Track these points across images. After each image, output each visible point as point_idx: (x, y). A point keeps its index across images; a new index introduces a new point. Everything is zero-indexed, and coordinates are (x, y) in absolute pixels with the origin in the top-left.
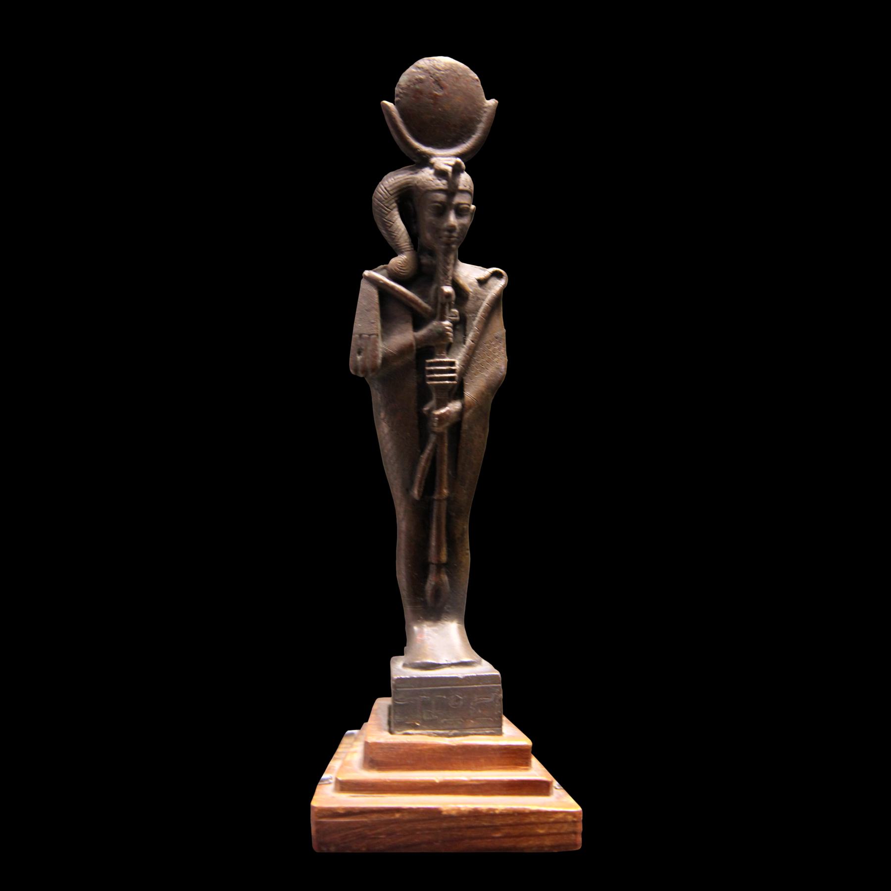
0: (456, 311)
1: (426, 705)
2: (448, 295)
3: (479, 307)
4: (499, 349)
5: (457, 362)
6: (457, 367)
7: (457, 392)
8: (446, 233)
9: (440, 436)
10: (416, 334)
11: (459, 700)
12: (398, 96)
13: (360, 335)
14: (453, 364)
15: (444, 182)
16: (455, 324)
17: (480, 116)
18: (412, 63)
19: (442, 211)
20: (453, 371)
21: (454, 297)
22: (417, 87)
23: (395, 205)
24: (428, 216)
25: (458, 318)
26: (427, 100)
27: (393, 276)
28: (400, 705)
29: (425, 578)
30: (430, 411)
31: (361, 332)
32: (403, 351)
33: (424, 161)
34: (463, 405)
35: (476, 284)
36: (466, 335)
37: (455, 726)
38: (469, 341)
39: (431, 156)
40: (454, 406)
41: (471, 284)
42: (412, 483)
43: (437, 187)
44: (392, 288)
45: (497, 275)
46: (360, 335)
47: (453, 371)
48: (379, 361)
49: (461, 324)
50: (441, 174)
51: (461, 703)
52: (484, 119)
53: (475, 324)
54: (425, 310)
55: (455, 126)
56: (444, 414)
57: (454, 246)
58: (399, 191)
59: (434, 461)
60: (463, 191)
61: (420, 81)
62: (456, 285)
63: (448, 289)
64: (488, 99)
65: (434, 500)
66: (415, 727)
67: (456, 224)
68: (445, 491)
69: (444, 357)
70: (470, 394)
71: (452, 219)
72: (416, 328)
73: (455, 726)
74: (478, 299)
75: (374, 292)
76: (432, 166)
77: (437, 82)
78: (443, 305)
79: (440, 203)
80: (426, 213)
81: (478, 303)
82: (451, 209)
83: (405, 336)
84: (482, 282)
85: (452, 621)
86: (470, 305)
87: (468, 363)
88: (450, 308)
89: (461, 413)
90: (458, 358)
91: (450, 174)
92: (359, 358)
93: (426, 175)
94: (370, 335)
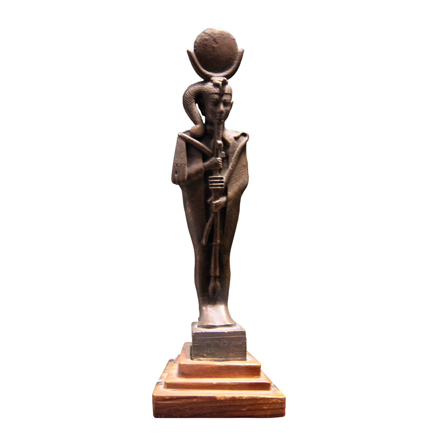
0: (224, 152)
1: (209, 346)
2: (220, 145)
3: (235, 151)
5: (224, 178)
6: (224, 180)
7: (224, 192)
8: (219, 114)
9: (216, 214)
10: (204, 164)
11: (225, 343)
14: (222, 178)
15: (218, 89)
16: (223, 159)
17: (235, 57)
19: (217, 103)
20: (222, 182)
21: (223, 146)
22: (205, 43)
23: (194, 100)
25: (225, 156)
26: (210, 49)
28: (196, 346)
29: (208, 283)
30: (211, 202)
31: (177, 163)
32: (198, 172)
33: (207, 79)
34: (227, 199)
35: (234, 139)
36: (228, 164)
37: (223, 356)
38: (230, 167)
39: (211, 76)
40: (223, 199)
41: (231, 139)
42: (202, 237)
43: (215, 92)
44: (192, 141)
47: (222, 182)
48: (186, 177)
49: (226, 159)
51: (226, 345)
53: (233, 159)
54: (209, 152)
55: (223, 62)
56: (218, 203)
58: (196, 94)
59: (213, 226)
60: (227, 94)
61: (206, 40)
62: (224, 140)
63: (220, 142)
65: (213, 245)
66: (204, 357)
67: (224, 110)
68: (218, 241)
69: (218, 175)
70: (230, 193)
72: (204, 161)
73: (223, 356)
74: (235, 147)
77: (215, 40)
78: (217, 150)
79: (216, 99)
80: (209, 105)
81: (235, 149)
82: (221, 103)
83: (198, 165)
85: (222, 304)
86: (230, 150)
87: (229, 178)
88: (221, 151)
89: (226, 203)
90: (224, 176)
91: (221, 85)
93: (209, 86)
94: (181, 164)
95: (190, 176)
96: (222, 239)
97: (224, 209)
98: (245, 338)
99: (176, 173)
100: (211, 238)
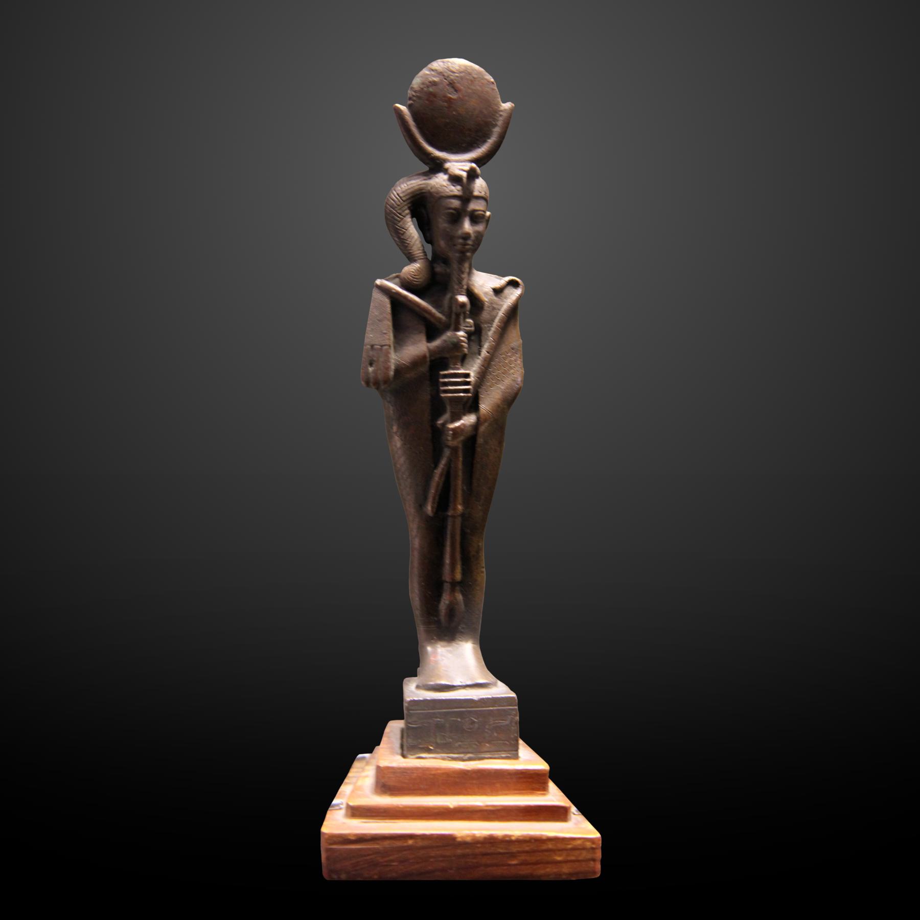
0: (471, 321)
1: (440, 727)
2: (463, 305)
3: (495, 317)
4: (516, 360)
5: (472, 374)
6: (471, 379)
7: (472, 405)
8: (461, 241)
9: (454, 450)
10: (429, 345)
11: (473, 722)
13: (372, 346)
14: (467, 376)
15: (459, 187)
16: (470, 335)
17: (495, 120)
19: (456, 217)
20: (468, 383)
21: (469, 307)
22: (431, 89)
23: (407, 211)
24: (442, 224)
25: (473, 329)
26: (441, 103)
27: (406, 285)
28: (413, 728)
29: (438, 596)
30: (444, 425)
31: (373, 343)
32: (417, 363)
33: (437, 166)
34: (478, 419)
35: (492, 293)
36: (481, 346)
37: (470, 750)
38: (484, 352)
39: (445, 161)
40: (469, 420)
41: (486, 293)
42: (425, 498)
43: (452, 193)
44: (405, 297)
46: (372, 346)
47: (468, 383)
48: (392, 373)
49: (476, 335)
51: (476, 726)
53: (490, 334)
54: (439, 320)
55: (470, 130)
56: (459, 427)
58: (412, 197)
59: (448, 476)
60: (478, 198)
61: (434, 84)
62: (471, 294)
63: (463, 299)
65: (448, 516)
66: (429, 751)
67: (471, 232)
68: (460, 507)
69: (458, 369)
70: (485, 407)
71: (467, 226)
72: (430, 338)
73: (470, 750)
74: (494, 309)
75: (387, 302)
76: (446, 171)
77: (452, 84)
78: (458, 315)
79: (455, 209)
80: (440, 220)
81: (494, 313)
82: (465, 216)
83: (418, 347)
84: (498, 291)
85: (467, 641)
86: (485, 315)
87: (483, 375)
88: (465, 318)
89: (476, 427)
90: (472, 370)
91: (465, 180)
92: (371, 369)
93: (440, 180)
94: (382, 346)
96: (466, 503)
97: (471, 439)
99: (371, 364)
100: (444, 502)
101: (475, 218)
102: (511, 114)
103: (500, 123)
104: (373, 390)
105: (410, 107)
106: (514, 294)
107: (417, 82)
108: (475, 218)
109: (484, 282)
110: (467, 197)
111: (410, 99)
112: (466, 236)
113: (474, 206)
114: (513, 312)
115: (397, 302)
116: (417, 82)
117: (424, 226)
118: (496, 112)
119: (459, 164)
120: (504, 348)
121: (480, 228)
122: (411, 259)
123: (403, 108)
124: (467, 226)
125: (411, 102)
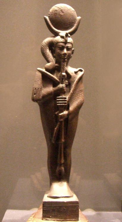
0: (67, 81)
1: (53, 210)
2: (64, 76)
3: (75, 80)
4: (82, 94)
5: (67, 98)
6: (67, 99)
7: (67, 108)
8: (63, 56)
9: (61, 122)
10: (53, 88)
11: (64, 209)
12: (47, 48)
13: (35, 88)
14: (65, 98)
15: (63, 39)
16: (67, 86)
17: (75, 21)
18: (54, 6)
19: (62, 48)
20: (66, 101)
21: (66, 76)
22: (55, 12)
23: (48, 47)
24: (58, 51)
25: (68, 84)
26: (58, 16)
27: (47, 70)
28: (45, 210)
29: (56, 168)
30: (58, 114)
31: (36, 87)
32: (50, 94)
33: (56, 34)
34: (69, 112)
35: (74, 73)
36: (70, 89)
37: (63, 218)
38: (71, 91)
39: (59, 33)
40: (65, 112)
41: (72, 73)
42: (52, 136)
43: (61, 41)
44: (46, 73)
45: (81, 71)
46: (35, 88)
47: (66, 101)
48: (41, 97)
49: (69, 85)
50: (62, 37)
51: (65, 210)
52: (76, 22)
53: (73, 86)
54: (57, 81)
55: (67, 24)
56: (62, 115)
57: (66, 60)
58: (49, 43)
59: (59, 130)
60: (69, 43)
61: (56, 10)
62: (67, 72)
63: (64, 74)
64: (78, 17)
65: (59, 143)
66: (49, 218)
67: (67, 53)
68: (63, 140)
69: (63, 96)
70: (71, 108)
71: (65, 51)
72: (54, 86)
73: (63, 218)
74: (75, 78)
75: (40, 74)
76: (60, 35)
77: (62, 11)
78: (63, 79)
79: (62, 46)
80: (57, 49)
81: (75, 79)
82: (65, 48)
83: (50, 89)
84: (76, 73)
85: (65, 182)
86: (71, 80)
87: (71, 98)
88: (65, 80)
89: (68, 115)
90: (67, 97)
91: (65, 37)
92: (35, 96)
93: (58, 39)
94: (38, 88)
95: (44, 97)
96: (65, 138)
97: (67, 119)
98: (78, 206)
99: (35, 94)
100: (58, 138)
101: (68, 49)
102: (80, 20)
103: (77, 22)
104: (36, 105)
105: (49, 17)
106: (80, 74)
107: (51, 10)
108: (68, 49)
109: (71, 70)
110: (66, 42)
111: (49, 15)
112: (65, 54)
113: (69, 45)
114: (81, 79)
115: (43, 74)
116: (51, 10)
117: (53, 52)
118: (75, 19)
119: (63, 33)
120: (78, 90)
121: (69, 52)
122: (48, 62)
123: (47, 18)
124: (65, 51)
125: (49, 16)
